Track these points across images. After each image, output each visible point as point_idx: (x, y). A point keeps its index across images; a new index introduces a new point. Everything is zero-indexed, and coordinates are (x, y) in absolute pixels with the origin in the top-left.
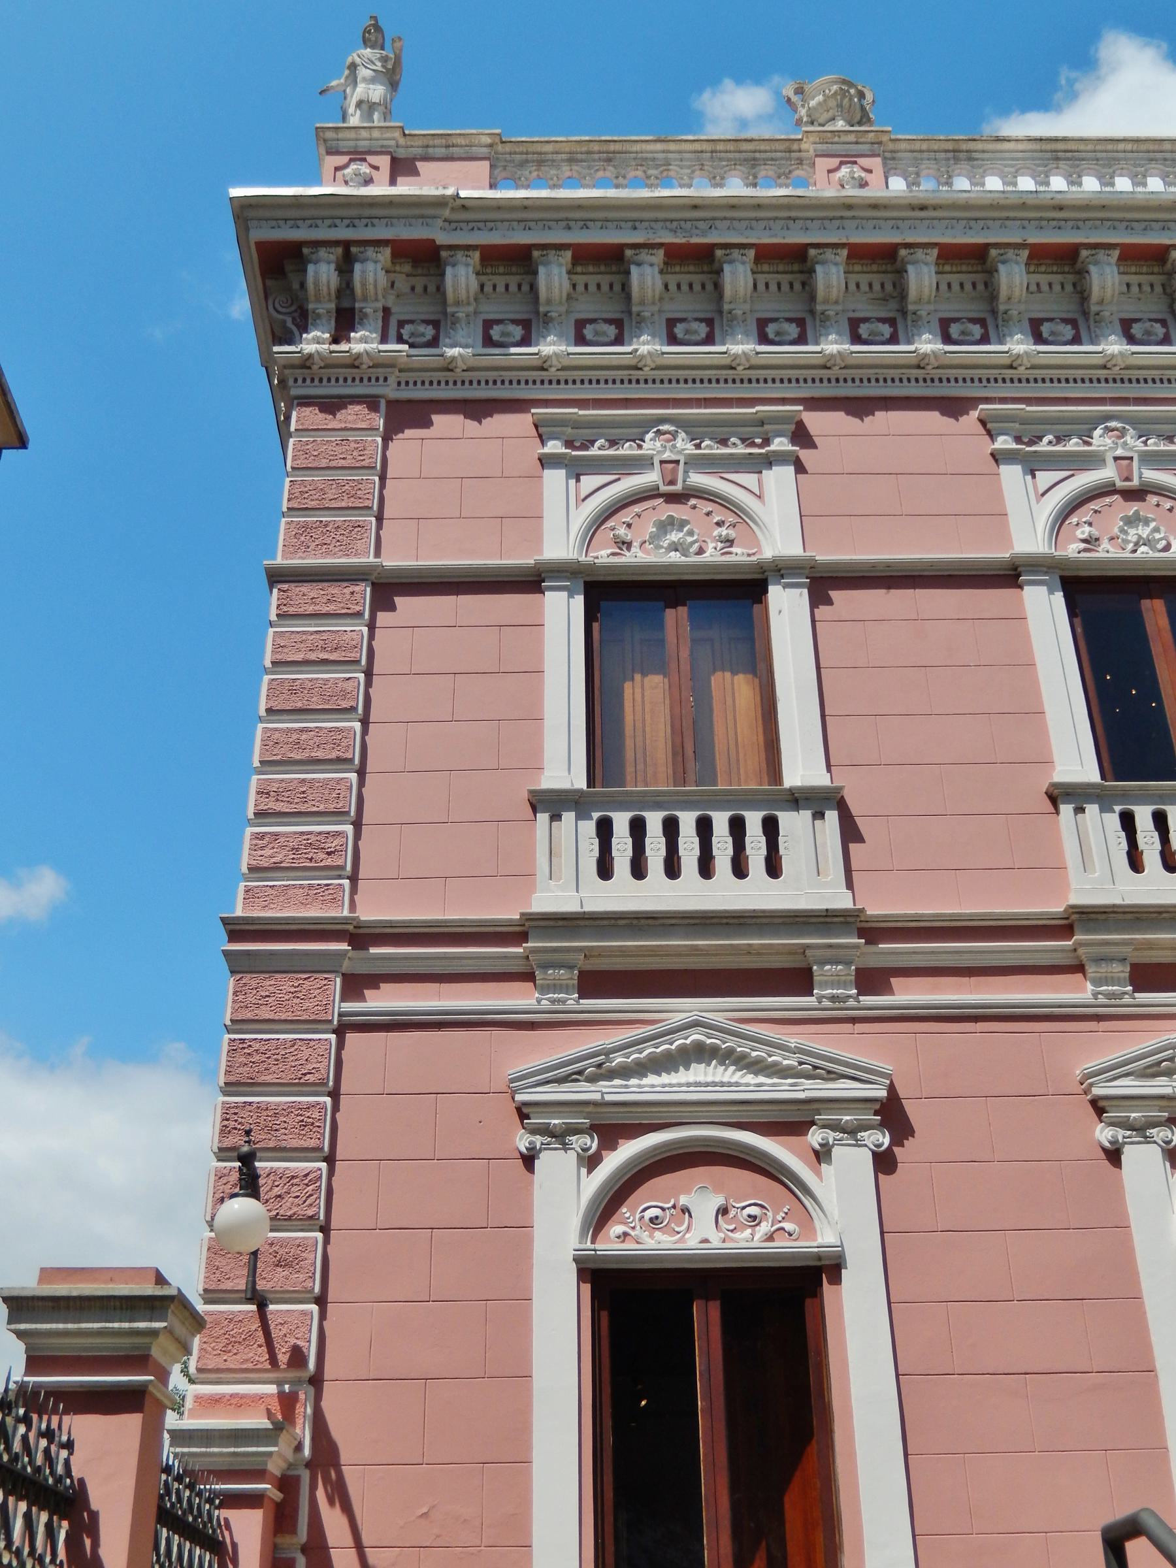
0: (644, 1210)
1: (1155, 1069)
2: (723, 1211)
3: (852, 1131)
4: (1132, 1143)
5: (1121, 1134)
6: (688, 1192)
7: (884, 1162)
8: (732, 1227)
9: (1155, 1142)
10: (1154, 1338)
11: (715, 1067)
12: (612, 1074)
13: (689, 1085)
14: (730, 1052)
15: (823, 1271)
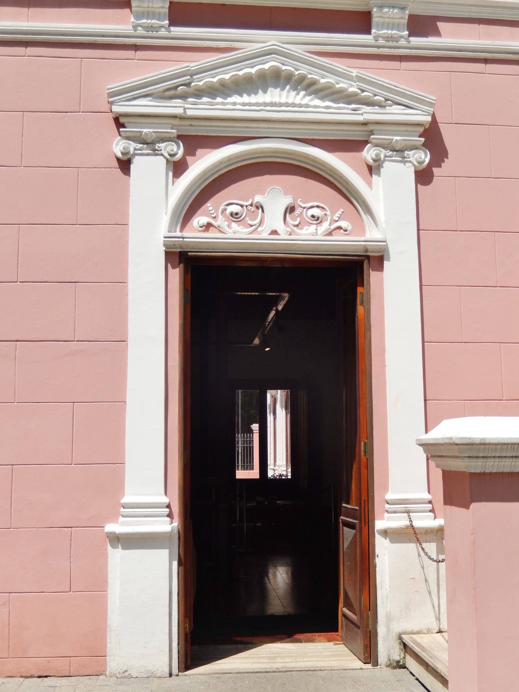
0: (228, 205)
1: (172, 92)
2: (291, 209)
3: (399, 151)
4: (142, 155)
5: (132, 146)
6: (262, 193)
7: (423, 176)
8: (297, 223)
9: (162, 155)
10: (130, 316)
11: (289, 92)
12: (199, 93)
13: (266, 104)
14: (302, 78)
15: (376, 259)
